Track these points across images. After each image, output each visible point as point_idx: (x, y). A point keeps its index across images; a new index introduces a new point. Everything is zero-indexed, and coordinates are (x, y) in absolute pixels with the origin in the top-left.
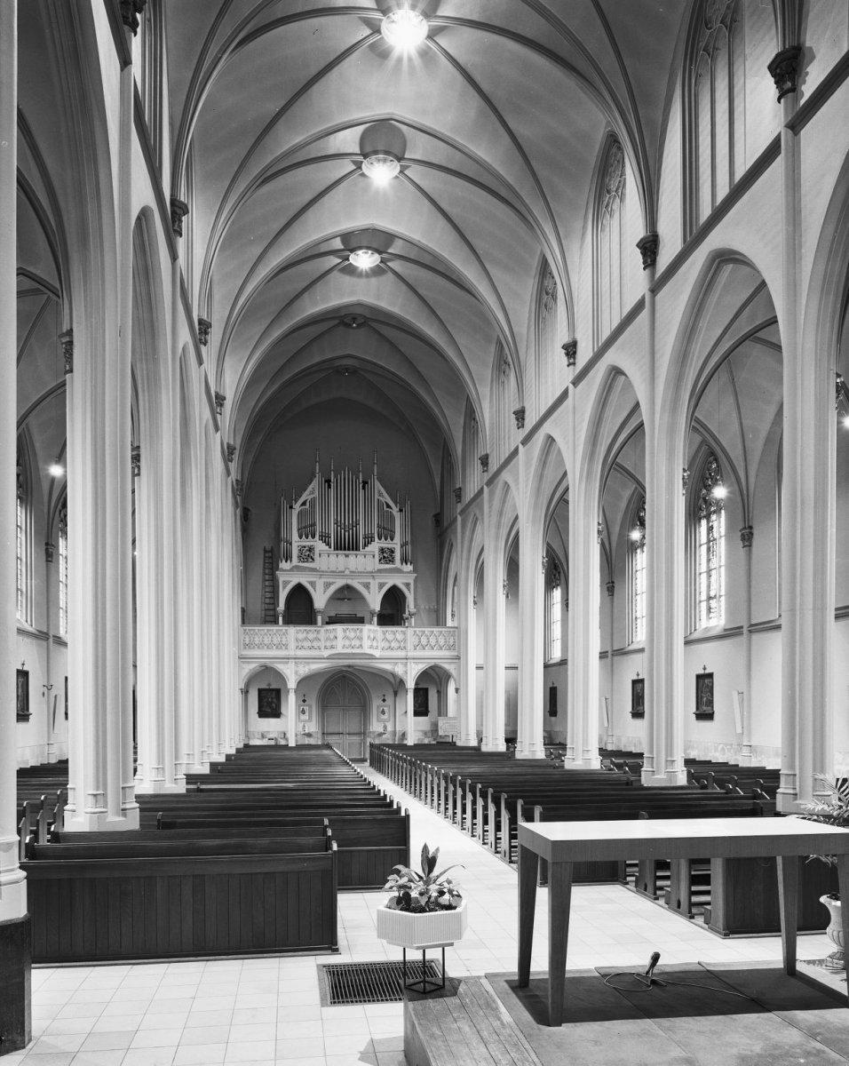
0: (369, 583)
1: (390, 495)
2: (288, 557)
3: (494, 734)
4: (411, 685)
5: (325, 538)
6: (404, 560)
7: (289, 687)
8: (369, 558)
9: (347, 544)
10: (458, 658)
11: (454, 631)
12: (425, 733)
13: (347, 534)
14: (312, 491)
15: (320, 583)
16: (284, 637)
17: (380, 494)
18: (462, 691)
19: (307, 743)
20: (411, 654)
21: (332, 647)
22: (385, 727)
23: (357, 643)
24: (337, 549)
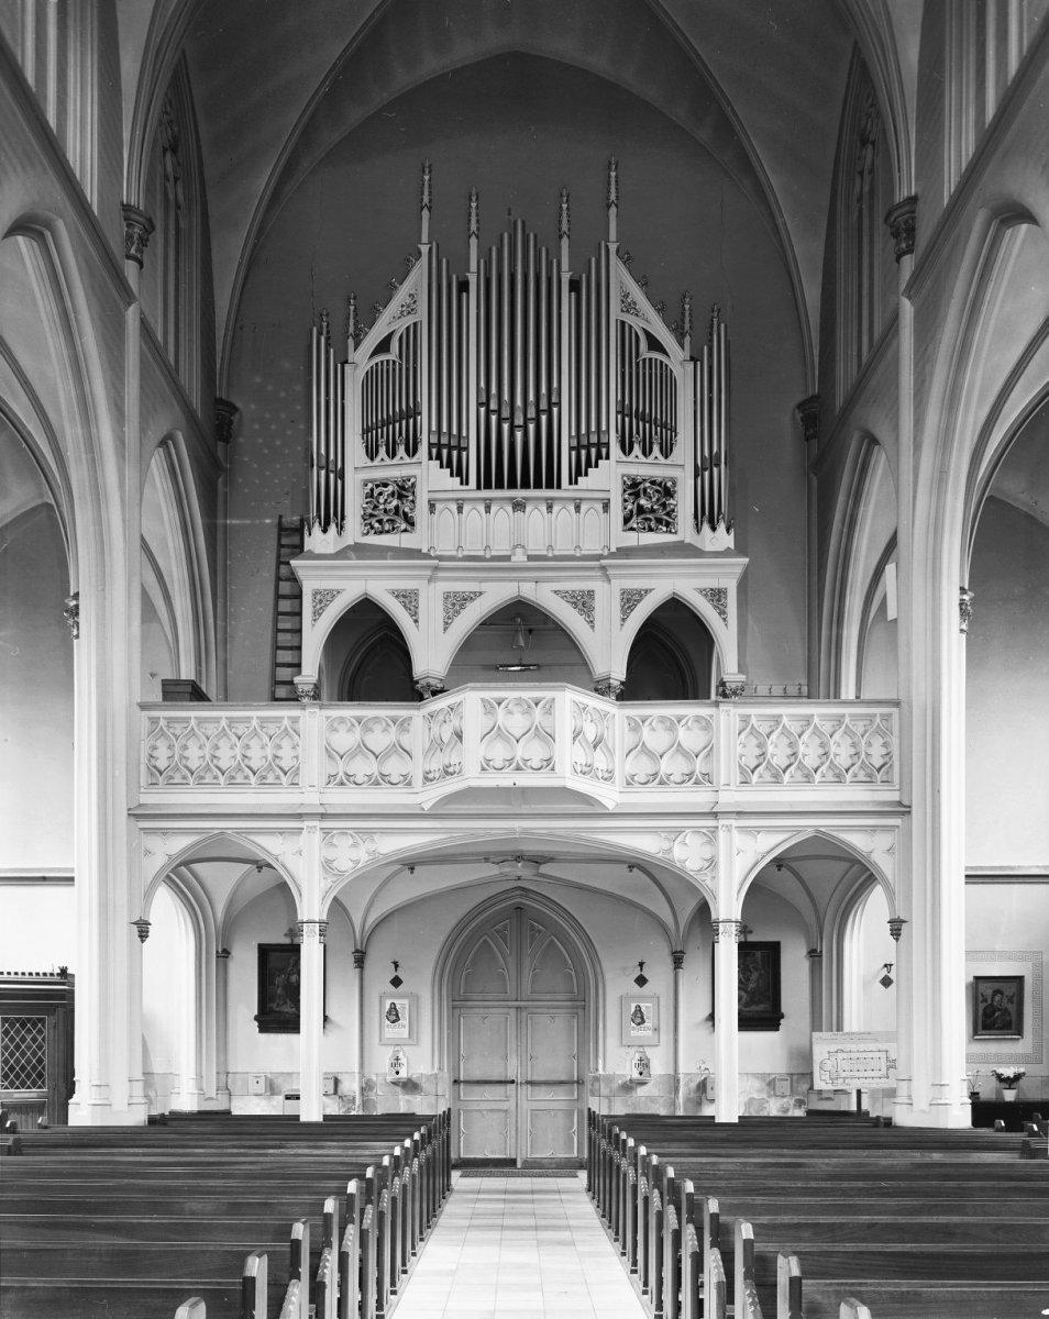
0: (591, 594)
1: (661, 308)
2: (332, 515)
3: (937, 1068)
4: (728, 906)
5: (448, 454)
6: (706, 515)
7: (303, 915)
8: (591, 512)
9: (519, 468)
10: (903, 810)
11: (886, 718)
12: (771, 1084)
13: (519, 435)
14: (406, 306)
15: (432, 599)
16: (286, 743)
17: (629, 307)
18: (915, 930)
19: (403, 1109)
20: (731, 798)
21: (447, 772)
22: (644, 1064)
23: (533, 751)
24: (488, 486)
